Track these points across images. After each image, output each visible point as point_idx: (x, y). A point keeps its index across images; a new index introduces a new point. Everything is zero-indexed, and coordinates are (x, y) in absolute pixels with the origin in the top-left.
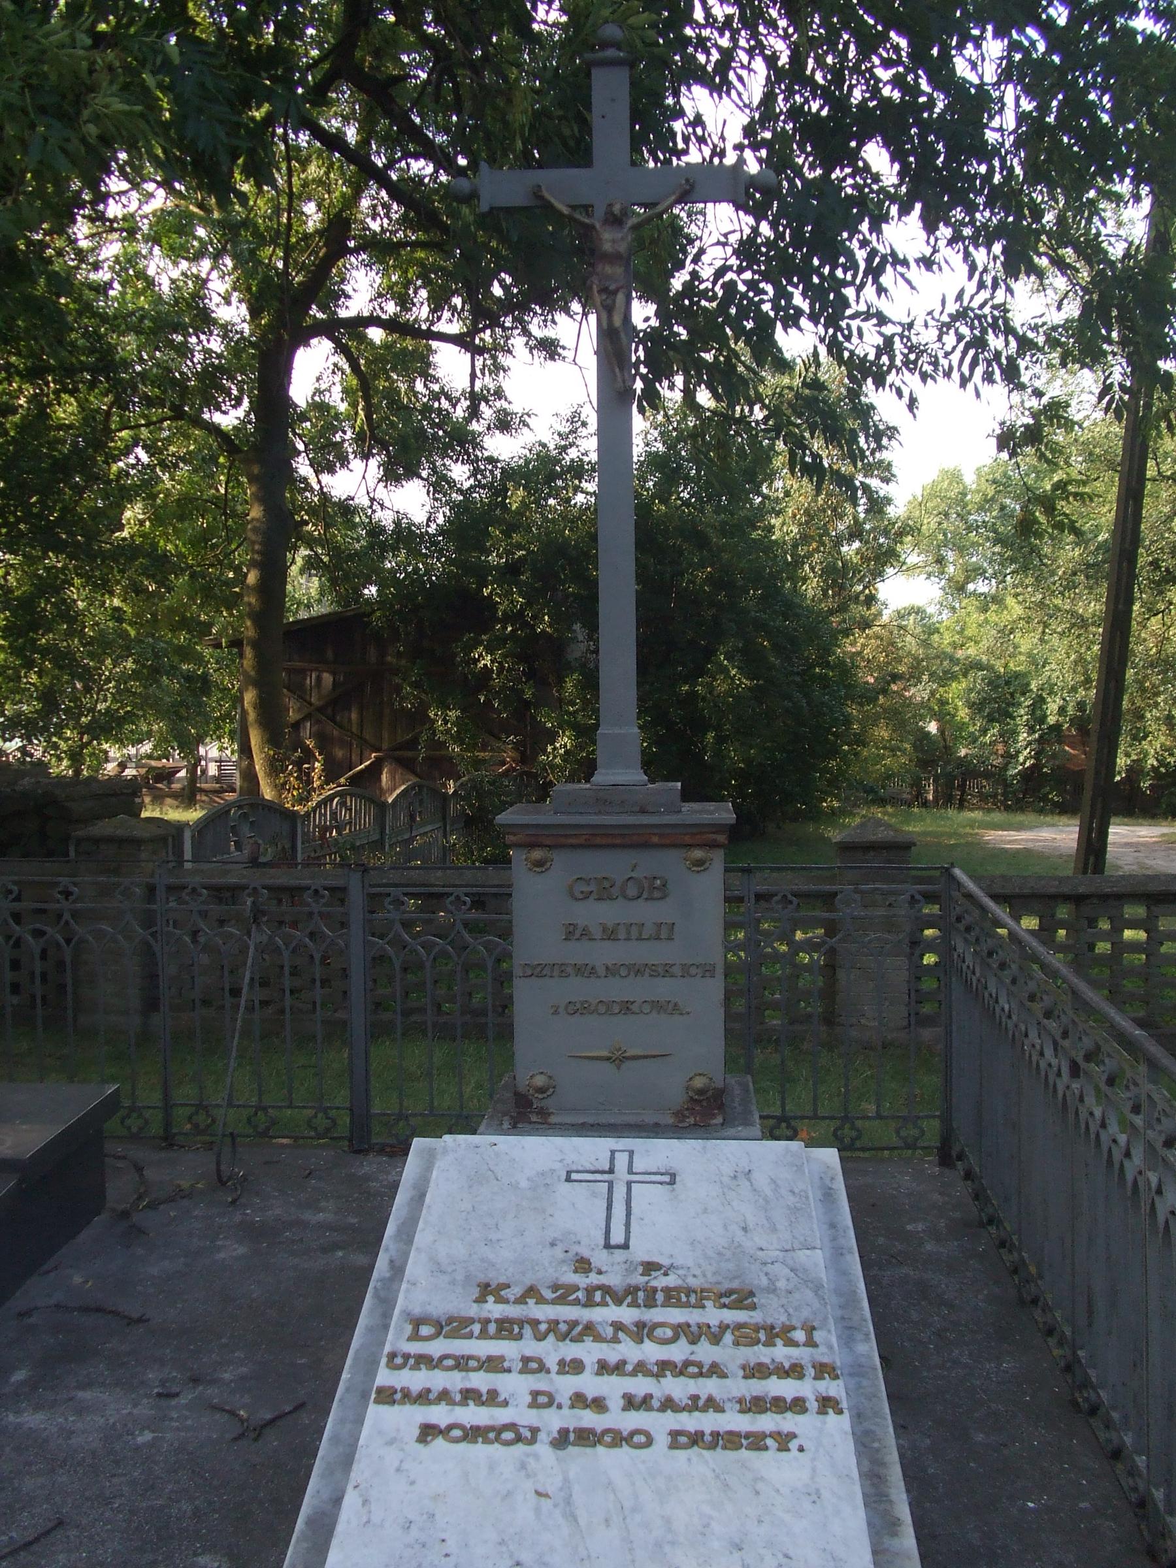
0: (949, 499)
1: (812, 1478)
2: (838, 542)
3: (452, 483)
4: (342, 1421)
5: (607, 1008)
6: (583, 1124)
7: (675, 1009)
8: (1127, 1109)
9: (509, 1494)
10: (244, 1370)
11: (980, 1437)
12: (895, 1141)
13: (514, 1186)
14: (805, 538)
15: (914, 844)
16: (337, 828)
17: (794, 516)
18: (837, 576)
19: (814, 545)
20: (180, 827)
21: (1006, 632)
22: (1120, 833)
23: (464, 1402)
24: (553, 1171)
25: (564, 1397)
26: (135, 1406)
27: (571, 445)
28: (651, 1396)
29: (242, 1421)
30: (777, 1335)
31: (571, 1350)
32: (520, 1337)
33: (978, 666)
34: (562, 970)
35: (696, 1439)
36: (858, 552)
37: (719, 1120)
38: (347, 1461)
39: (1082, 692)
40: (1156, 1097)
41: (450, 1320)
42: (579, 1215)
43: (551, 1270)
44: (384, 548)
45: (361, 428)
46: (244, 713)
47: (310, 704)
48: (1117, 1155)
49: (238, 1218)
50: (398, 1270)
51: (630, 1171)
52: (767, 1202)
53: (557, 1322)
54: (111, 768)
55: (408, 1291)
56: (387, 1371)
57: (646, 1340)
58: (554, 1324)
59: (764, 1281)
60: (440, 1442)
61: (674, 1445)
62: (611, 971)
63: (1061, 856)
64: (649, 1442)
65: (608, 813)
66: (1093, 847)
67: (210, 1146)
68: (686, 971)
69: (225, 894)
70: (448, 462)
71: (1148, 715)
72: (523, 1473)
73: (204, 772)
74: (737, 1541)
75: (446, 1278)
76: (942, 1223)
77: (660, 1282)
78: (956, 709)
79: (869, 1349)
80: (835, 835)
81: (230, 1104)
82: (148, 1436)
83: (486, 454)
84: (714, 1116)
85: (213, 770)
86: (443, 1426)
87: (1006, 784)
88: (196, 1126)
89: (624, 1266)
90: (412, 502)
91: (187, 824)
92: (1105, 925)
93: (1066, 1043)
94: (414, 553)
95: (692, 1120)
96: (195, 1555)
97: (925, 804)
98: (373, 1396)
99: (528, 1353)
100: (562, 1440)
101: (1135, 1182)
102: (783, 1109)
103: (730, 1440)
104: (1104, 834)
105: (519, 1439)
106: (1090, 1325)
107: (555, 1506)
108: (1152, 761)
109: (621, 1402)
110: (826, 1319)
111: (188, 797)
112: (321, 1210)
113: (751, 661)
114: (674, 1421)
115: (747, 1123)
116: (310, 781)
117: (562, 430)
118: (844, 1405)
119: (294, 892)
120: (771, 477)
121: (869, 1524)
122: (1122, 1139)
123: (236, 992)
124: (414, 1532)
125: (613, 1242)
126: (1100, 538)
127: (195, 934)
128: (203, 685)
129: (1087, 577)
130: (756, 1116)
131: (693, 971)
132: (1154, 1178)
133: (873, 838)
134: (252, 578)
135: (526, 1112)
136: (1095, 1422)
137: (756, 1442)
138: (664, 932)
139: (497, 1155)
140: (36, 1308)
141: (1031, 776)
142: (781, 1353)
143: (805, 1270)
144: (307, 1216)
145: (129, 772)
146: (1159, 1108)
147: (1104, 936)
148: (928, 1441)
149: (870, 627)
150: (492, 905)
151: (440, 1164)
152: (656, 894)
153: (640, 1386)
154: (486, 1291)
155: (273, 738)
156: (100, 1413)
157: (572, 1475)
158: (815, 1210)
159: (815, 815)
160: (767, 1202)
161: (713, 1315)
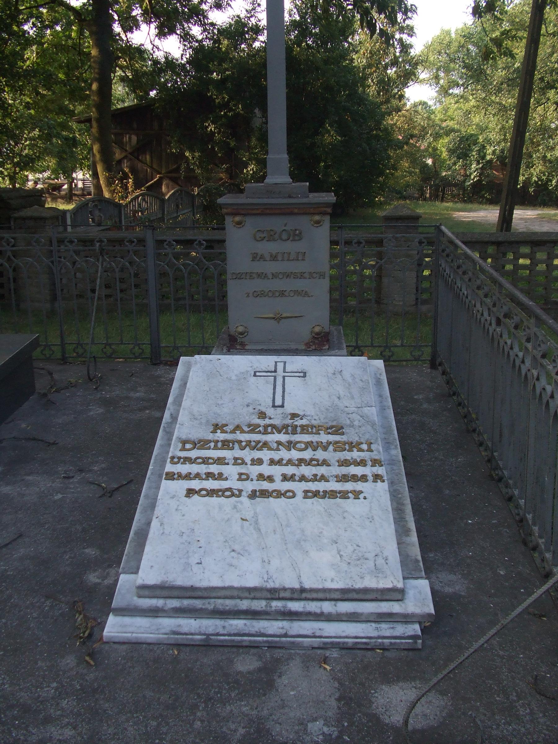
0: (442, 44)
1: (370, 511)
2: (386, 67)
3: (193, 37)
4: (150, 488)
5: (273, 294)
6: (262, 350)
7: (306, 294)
8: (523, 341)
9: (228, 520)
10: (103, 465)
11: (447, 492)
12: (409, 356)
13: (230, 379)
14: (369, 66)
15: (421, 217)
16: (141, 211)
17: (364, 54)
18: (385, 85)
19: (374, 69)
20: (64, 212)
21: (468, 113)
22: (519, 213)
23: (207, 479)
24: (247, 372)
25: (254, 476)
26: (53, 482)
27: (252, 16)
28: (295, 475)
29: (104, 489)
30: (354, 447)
31: (257, 454)
32: (233, 448)
33: (453, 130)
34: (250, 276)
35: (316, 494)
36: (395, 72)
37: (327, 347)
38: (153, 506)
39: (503, 144)
40: (538, 334)
41: (200, 441)
42: (260, 392)
43: (247, 418)
44: (161, 71)
45: (146, 8)
46: (94, 155)
47: (126, 151)
48: (518, 362)
49: (99, 396)
50: (174, 418)
51: (284, 372)
52: (350, 385)
53: (250, 442)
54: (30, 184)
55: (179, 428)
56: (170, 465)
57: (292, 449)
58: (249, 442)
59: (348, 422)
60: (196, 496)
61: (306, 497)
62: (274, 276)
63: (489, 224)
64: (294, 496)
65: (273, 198)
66: (506, 220)
67: (84, 363)
68: (311, 275)
69: (86, 242)
70: (190, 25)
71: (534, 156)
72: (235, 510)
73: (76, 185)
74: (335, 539)
75: (198, 422)
76: (431, 395)
77: (299, 422)
78: (441, 152)
79: (397, 453)
80: (381, 213)
82: (60, 496)
83: (210, 21)
84: (324, 345)
85: (80, 185)
86: (197, 490)
87: (464, 190)
88: (77, 353)
89: (281, 415)
90: (173, 47)
91: (68, 210)
92: (510, 256)
93: (495, 309)
94: (174, 72)
95: (314, 347)
96: (84, 548)
97: (425, 199)
98: (164, 476)
99: (237, 456)
100: (253, 495)
101: (526, 375)
102: (357, 342)
103: (332, 494)
104: (511, 214)
105: (233, 495)
106: (500, 441)
107: (251, 525)
108: (535, 179)
109: (281, 478)
110: (377, 438)
111: (69, 198)
112: (138, 392)
113: (342, 129)
114: (305, 486)
115: (340, 348)
116: (127, 188)
117: (248, 8)
118: (385, 478)
119: (120, 242)
120: (353, 33)
121: (396, 531)
122: (521, 354)
123: (93, 291)
124: (185, 537)
125: (276, 404)
126: (516, 66)
127: (74, 263)
128: (74, 142)
129: (508, 86)
130: (345, 345)
131: (315, 275)
132: (535, 372)
133: (401, 214)
134: (95, 86)
135: (234, 344)
136: (501, 485)
137: (344, 495)
138: (301, 256)
139: (221, 364)
140: (4, 439)
141: (477, 186)
142: (356, 455)
143: (367, 417)
144: (132, 394)
145: (40, 186)
146: (540, 339)
147: (509, 262)
148: (423, 494)
149: (400, 111)
150: (216, 247)
151: (193, 369)
152: (297, 238)
153: (290, 470)
154: (217, 427)
155: (108, 168)
156: (37, 486)
157: (258, 510)
158: (372, 388)
159: (373, 204)
160: (350, 385)
161: (324, 438)
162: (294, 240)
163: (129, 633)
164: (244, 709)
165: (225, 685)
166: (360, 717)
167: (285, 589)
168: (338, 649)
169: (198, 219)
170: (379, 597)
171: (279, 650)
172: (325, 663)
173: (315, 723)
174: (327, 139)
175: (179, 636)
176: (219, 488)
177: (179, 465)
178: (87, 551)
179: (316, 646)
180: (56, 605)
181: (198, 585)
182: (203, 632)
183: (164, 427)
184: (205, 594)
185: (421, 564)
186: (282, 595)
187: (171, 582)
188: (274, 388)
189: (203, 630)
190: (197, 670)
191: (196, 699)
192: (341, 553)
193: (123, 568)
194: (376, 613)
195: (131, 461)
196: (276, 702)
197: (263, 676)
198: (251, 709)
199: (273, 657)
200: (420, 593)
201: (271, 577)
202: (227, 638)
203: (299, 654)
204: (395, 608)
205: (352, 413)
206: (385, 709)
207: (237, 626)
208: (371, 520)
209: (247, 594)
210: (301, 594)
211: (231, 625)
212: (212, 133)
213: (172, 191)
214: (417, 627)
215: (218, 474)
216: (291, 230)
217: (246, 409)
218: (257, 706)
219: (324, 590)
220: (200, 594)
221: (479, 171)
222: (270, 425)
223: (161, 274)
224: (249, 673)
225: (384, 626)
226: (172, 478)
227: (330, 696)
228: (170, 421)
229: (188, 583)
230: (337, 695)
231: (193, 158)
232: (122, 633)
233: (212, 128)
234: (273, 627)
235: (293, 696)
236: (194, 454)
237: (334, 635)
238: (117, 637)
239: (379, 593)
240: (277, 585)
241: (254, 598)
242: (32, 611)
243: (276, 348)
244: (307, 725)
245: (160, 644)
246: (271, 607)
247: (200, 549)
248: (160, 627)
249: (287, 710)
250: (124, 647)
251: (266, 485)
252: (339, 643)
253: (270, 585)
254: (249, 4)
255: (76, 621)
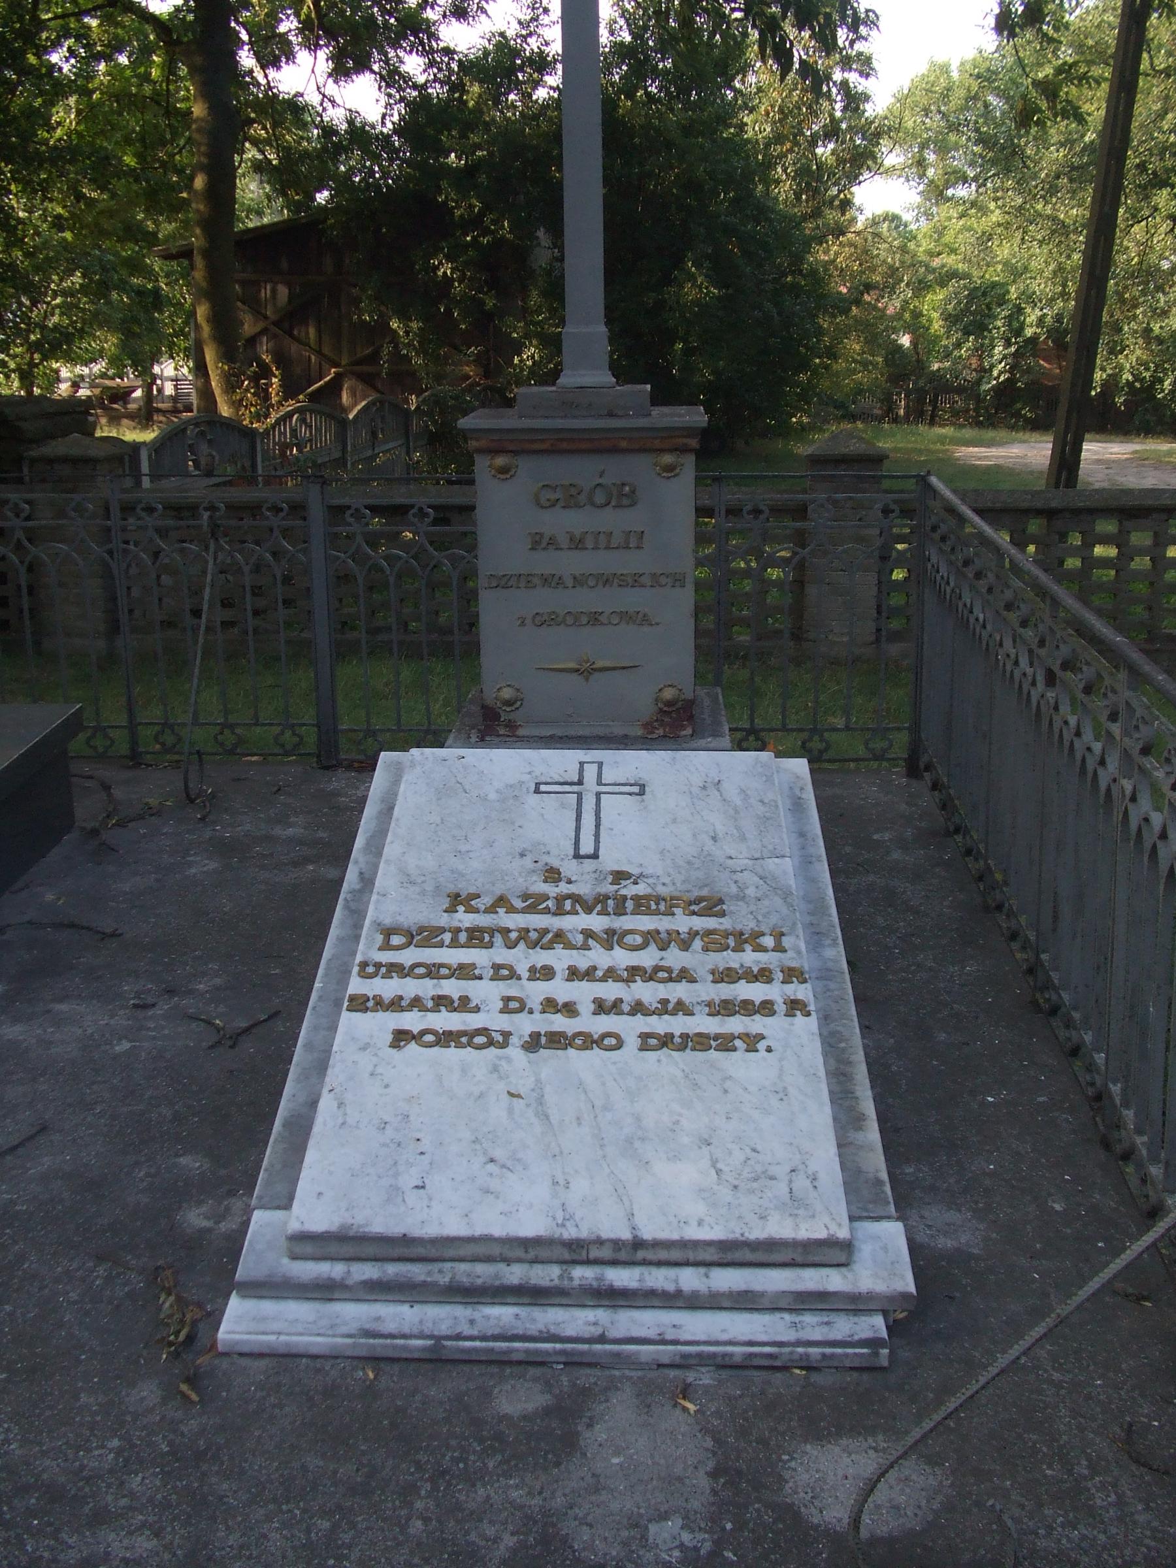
0: (932, 93)
1: (780, 1077)
2: (813, 142)
3: (407, 78)
4: (315, 1028)
5: (575, 619)
6: (552, 737)
7: (646, 620)
8: (1103, 718)
9: (481, 1095)
10: (218, 981)
11: (942, 1036)
12: (861, 751)
13: (484, 799)
14: (778, 139)
15: (887, 457)
16: (297, 445)
17: (767, 114)
18: (812, 178)
19: (788, 145)
20: (136, 447)
21: (986, 238)
22: (1093, 450)
23: (436, 1009)
24: (521, 783)
25: (535, 1002)
26: (112, 1017)
27: (530, 35)
28: (621, 1001)
29: (218, 1030)
30: (746, 942)
31: (542, 958)
32: (490, 945)
33: (954, 274)
34: (527, 581)
35: (666, 1041)
36: (833, 152)
37: (689, 731)
38: (321, 1066)
39: (1060, 304)
40: (1135, 703)
41: (421, 930)
42: (549, 826)
43: (521, 880)
44: (339, 149)
45: (308, 16)
46: (198, 327)
47: (266, 317)
48: (1091, 764)
49: (208, 834)
50: (367, 881)
51: (599, 783)
52: (737, 812)
53: (527, 931)
54: (64, 388)
55: (378, 901)
56: (359, 980)
57: (616, 947)
58: (524, 932)
59: (734, 889)
60: (413, 1045)
61: (644, 1048)
62: (578, 581)
63: (1032, 473)
64: (619, 1045)
65: (575, 417)
66: (1066, 463)
67: (176, 764)
68: (656, 580)
69: (182, 510)
70: (401, 54)
71: (1126, 328)
72: (495, 1075)
73: (160, 390)
74: (706, 1136)
75: (417, 889)
77: (629, 890)
78: (930, 321)
79: (836, 954)
80: (803, 450)
81: (196, 722)
82: (126, 1045)
83: (442, 45)
84: (683, 728)
85: (169, 389)
86: (415, 1032)
87: (979, 400)
88: (163, 744)
89: (593, 875)
90: (364, 99)
91: (144, 443)
92: (1076, 540)
93: (1042, 652)
94: (367, 153)
95: (661, 732)
96: (177, 1155)
97: (896, 420)
98: (346, 1004)
99: (499, 961)
100: (534, 1043)
101: (1109, 790)
102: (752, 721)
103: (700, 1042)
104: (1078, 450)
105: (491, 1043)
106: (1054, 930)
107: (528, 1105)
108: (1127, 376)
109: (592, 1007)
110: (794, 924)
111: (145, 416)
112: (290, 825)
113: (721, 271)
114: (642, 1024)
115: (716, 734)
116: (267, 397)
117: (522, 17)
118: (812, 1008)
119: (254, 509)
120: (744, 70)
121: (835, 1119)
122: (1097, 747)
123: (197, 613)
124: (389, 1131)
125: (582, 852)
126: (1087, 139)
127: (156, 555)
128: (156, 300)
129: (1071, 180)
130: (726, 728)
131: (663, 580)
132: (1127, 785)
133: (845, 451)
134: (199, 182)
135: (494, 725)
136: (1056, 1022)
137: (726, 1043)
138: (633, 540)
139: (465, 767)
140: (9, 926)
141: (1005, 391)
142: (750, 958)
143: (774, 878)
144: (278, 831)
145: (83, 393)
146: (1138, 714)
147: (1074, 552)
148: (892, 1041)
149: (843, 234)
150: (454, 521)
151: (407, 777)
152: (625, 501)
153: (611, 991)
154: (456, 900)
155: (228, 354)
156: (78, 1024)
157: (543, 1076)
158: (784, 818)
159: (785, 431)
160: (737, 812)
161: (682, 922)
162: (619, 506)
163: (273, 1333)
164: (515, 1494)
165: (475, 1444)
166: (758, 1510)
167: (600, 1242)
168: (712, 1368)
169: (418, 462)
170: (799, 1259)
171: (588, 1371)
172: (684, 1398)
173: (663, 1524)
174: (690, 292)
175: (377, 1341)
176: (462, 1028)
177: (377, 981)
178: (183, 1161)
179: (666, 1361)
180: (119, 1275)
181: (417, 1232)
182: (427, 1332)
183: (346, 899)
184: (433, 1252)
185: (888, 1189)
186: (595, 1253)
187: (360, 1226)
188: (578, 819)
189: (428, 1328)
190: (414, 1413)
191: (412, 1474)
192: (719, 1166)
193: (260, 1198)
194: (792, 1292)
195: (277, 971)
196: (583, 1479)
197: (554, 1425)
198: (529, 1493)
199: (574, 1385)
200: (885, 1249)
201: (571, 1217)
202: (477, 1344)
203: (629, 1378)
204: (833, 1281)
205: (742, 871)
206: (810, 1495)
207: (498, 1318)
208: (781, 1095)
209: (520, 1253)
210: (634, 1251)
211: (487, 1318)
212: (447, 281)
213: (363, 403)
214: (879, 1321)
215: (460, 998)
216: (614, 484)
217: (518, 863)
218: (542, 1488)
219: (683, 1244)
220: (421, 1251)
221: (1009, 361)
222: (569, 896)
223: (338, 577)
224: (525, 1417)
225: (809, 1319)
226: (362, 1007)
227: (696, 1468)
228: (358, 887)
229: (395, 1229)
230: (711, 1464)
231: (407, 333)
232: (257, 1334)
233: (446, 269)
234: (576, 1321)
235: (618, 1468)
236: (408, 957)
237: (703, 1338)
238: (247, 1342)
239: (800, 1250)
240: (584, 1234)
241: (535, 1261)
242: (68, 1288)
243: (581, 733)
244: (647, 1528)
245: (337, 1357)
246: (571, 1279)
247: (423, 1157)
248: (338, 1321)
249: (604, 1496)
250: (262, 1363)
251: (560, 1023)
252: (714, 1355)
253: (570, 1233)
254: (524, 9)
255: (159, 1308)
